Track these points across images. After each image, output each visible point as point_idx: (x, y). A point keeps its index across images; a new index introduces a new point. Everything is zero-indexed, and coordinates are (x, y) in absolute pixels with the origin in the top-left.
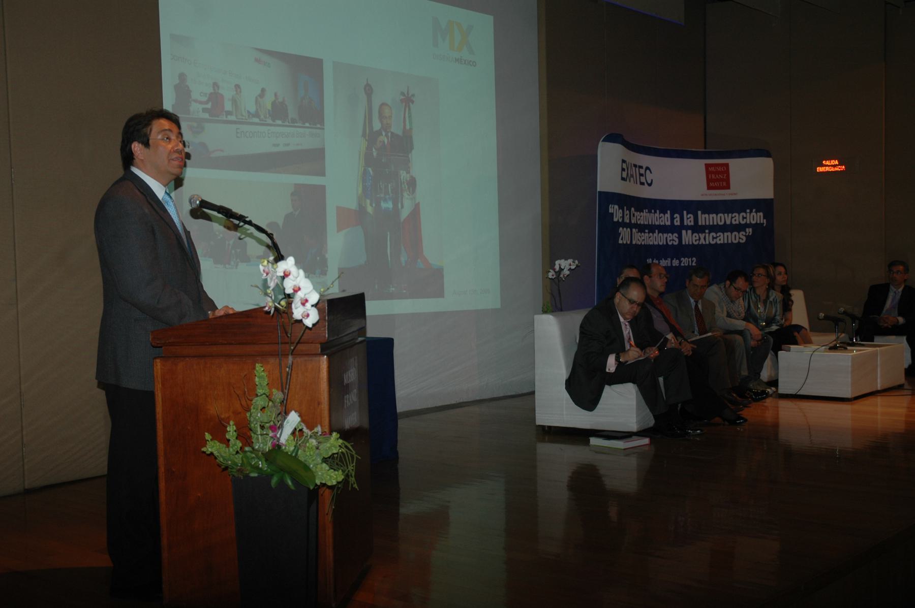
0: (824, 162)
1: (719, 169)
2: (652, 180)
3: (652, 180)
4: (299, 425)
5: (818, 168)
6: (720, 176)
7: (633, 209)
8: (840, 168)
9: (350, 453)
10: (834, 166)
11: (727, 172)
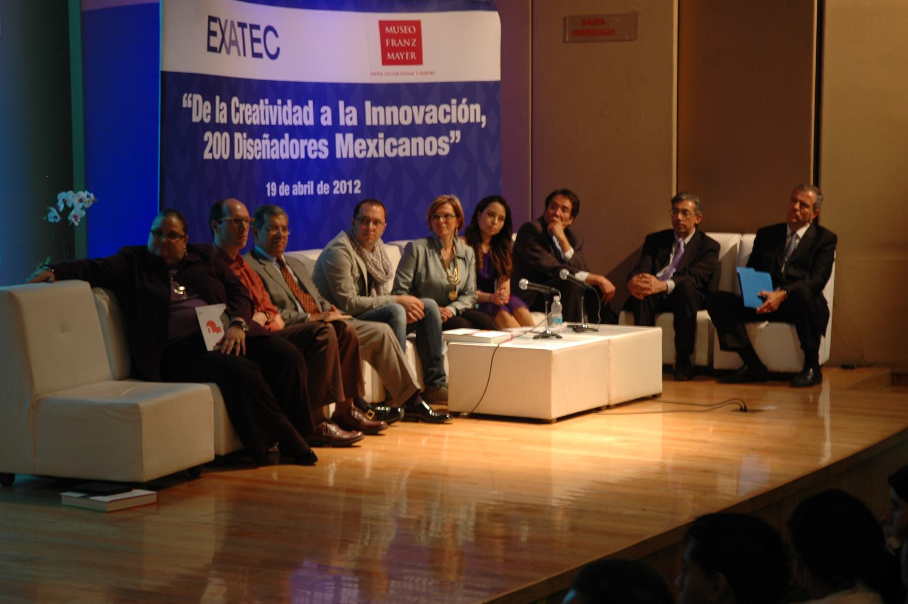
1: (405, 30)
2: (278, 49)
3: (278, 49)
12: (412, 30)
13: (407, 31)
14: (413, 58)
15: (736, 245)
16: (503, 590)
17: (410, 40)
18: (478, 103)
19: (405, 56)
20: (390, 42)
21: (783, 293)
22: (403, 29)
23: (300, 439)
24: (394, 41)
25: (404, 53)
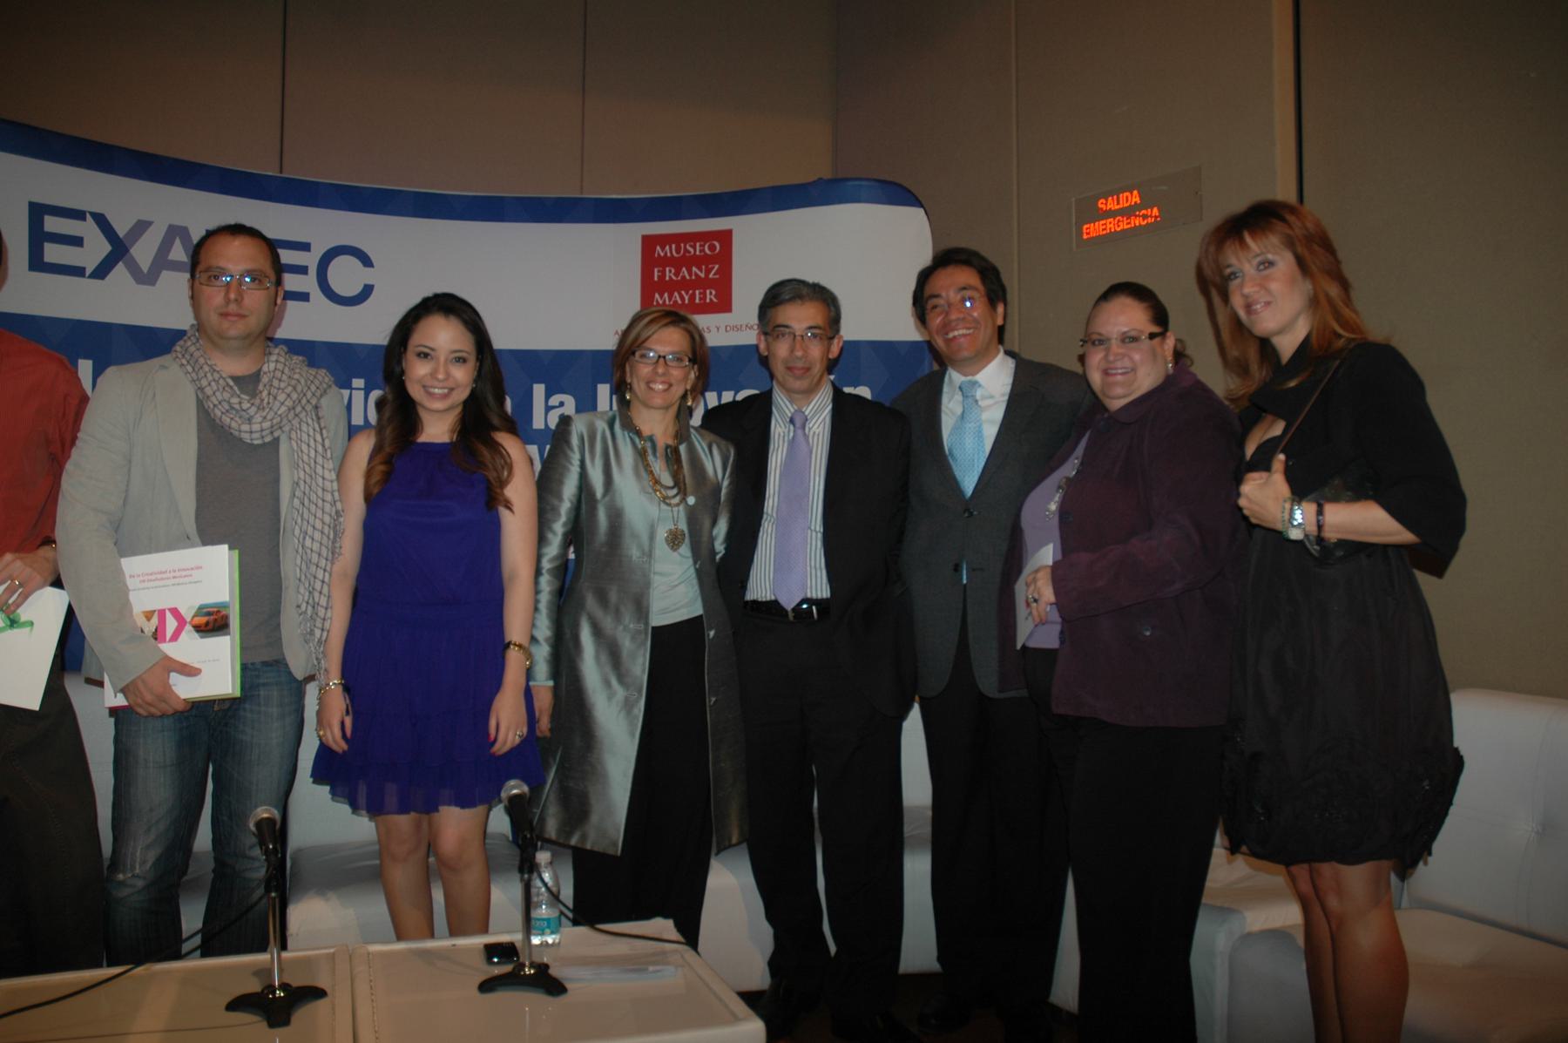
1: (696, 250)
2: (116, 696)
3: (116, 696)
4: (791, 330)
5: (1085, 226)
6: (662, 254)
8: (1145, 217)
9: (701, 271)
10: (1128, 212)
11: (725, 259)
12: (712, 248)
13: (702, 250)
14: (711, 299)
15: (717, 854)
16: (1129, 395)
17: (706, 267)
19: (692, 298)
20: (663, 272)
21: (969, 481)
24: (670, 271)
25: (691, 292)
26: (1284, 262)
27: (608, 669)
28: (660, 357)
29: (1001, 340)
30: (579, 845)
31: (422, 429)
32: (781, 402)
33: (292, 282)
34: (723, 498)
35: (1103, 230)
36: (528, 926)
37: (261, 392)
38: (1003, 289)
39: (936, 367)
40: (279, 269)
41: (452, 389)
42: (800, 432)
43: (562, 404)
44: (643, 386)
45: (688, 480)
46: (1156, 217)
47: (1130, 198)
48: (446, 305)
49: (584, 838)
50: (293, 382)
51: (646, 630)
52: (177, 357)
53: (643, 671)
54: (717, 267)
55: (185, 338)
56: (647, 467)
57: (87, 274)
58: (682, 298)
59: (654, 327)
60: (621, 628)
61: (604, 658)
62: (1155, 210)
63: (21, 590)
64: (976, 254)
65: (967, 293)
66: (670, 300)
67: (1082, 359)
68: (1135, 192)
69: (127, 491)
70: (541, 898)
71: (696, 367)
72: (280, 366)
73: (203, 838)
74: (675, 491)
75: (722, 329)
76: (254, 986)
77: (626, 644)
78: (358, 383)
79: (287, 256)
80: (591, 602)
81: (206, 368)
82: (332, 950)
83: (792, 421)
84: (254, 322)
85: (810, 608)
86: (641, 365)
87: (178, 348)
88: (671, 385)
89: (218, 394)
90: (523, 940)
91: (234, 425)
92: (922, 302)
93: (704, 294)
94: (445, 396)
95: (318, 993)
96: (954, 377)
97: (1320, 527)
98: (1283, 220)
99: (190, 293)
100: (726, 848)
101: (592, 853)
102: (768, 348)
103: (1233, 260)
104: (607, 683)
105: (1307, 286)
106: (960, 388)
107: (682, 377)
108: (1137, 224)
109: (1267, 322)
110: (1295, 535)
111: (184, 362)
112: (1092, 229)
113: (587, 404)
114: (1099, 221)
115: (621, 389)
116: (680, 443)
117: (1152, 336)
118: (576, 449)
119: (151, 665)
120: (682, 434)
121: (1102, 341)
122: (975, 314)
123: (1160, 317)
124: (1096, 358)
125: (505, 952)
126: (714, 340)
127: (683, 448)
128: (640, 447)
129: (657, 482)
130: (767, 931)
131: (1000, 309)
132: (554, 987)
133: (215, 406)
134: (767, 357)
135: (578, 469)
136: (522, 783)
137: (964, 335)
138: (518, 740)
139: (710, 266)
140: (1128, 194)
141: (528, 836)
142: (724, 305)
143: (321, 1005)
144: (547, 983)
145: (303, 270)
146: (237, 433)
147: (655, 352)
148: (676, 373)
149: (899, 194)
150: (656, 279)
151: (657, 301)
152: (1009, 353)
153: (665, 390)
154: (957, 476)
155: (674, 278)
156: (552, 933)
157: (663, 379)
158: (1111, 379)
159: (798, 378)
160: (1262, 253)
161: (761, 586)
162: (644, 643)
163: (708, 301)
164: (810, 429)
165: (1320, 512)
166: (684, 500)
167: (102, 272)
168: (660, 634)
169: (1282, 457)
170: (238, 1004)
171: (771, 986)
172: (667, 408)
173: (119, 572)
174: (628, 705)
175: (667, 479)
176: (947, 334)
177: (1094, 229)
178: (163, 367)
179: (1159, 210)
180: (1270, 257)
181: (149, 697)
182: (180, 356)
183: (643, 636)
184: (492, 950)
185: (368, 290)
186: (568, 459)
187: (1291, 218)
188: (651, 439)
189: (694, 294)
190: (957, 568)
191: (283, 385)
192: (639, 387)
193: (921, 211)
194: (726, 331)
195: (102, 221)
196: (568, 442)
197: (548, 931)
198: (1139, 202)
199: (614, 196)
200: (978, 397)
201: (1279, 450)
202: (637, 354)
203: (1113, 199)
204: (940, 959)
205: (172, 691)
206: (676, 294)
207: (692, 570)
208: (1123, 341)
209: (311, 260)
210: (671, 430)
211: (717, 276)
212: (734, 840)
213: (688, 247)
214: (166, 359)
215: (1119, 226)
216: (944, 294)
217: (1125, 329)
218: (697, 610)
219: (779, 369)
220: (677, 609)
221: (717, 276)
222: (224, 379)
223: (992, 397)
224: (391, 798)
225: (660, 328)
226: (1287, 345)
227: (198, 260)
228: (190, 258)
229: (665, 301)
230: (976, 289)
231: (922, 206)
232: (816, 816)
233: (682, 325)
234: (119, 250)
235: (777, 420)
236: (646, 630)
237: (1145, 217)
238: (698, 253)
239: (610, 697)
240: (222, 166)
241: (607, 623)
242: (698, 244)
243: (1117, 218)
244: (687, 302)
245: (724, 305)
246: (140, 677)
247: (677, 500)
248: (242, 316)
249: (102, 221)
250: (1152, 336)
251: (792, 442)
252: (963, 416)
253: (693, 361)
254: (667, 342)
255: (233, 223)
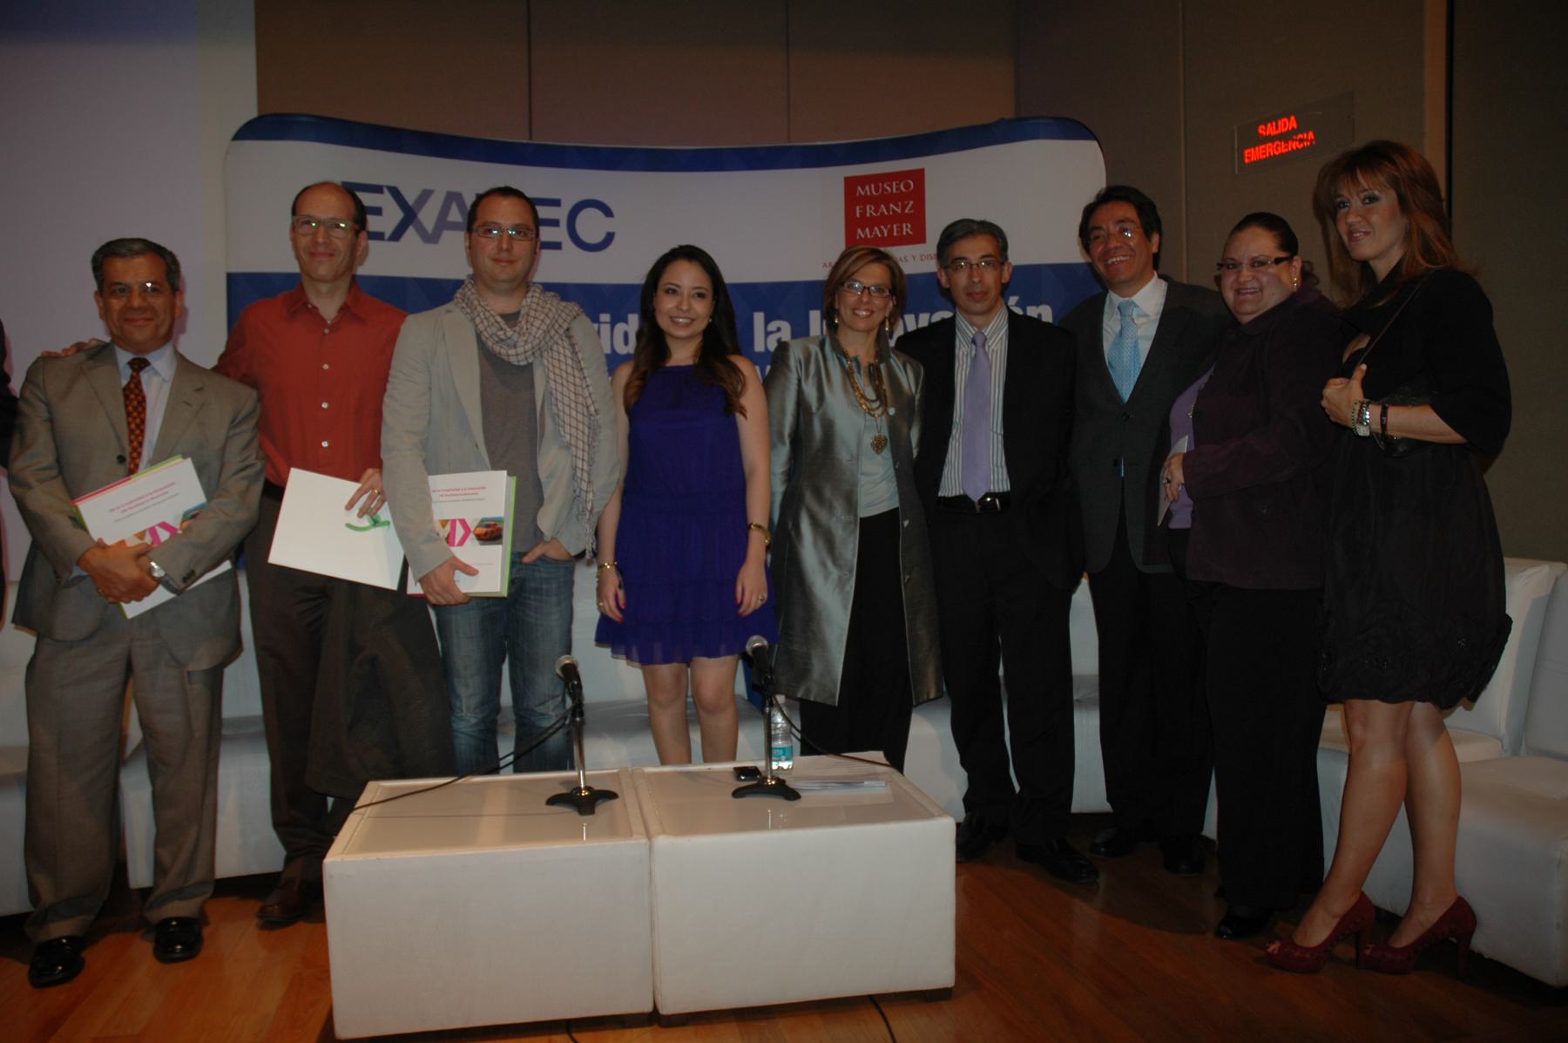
0: (1261, 130)
5: (1246, 152)
6: (863, 236)
7: (1294, 137)
8: (1301, 141)
10: (1286, 137)
11: (918, 195)
12: (907, 186)
13: (898, 189)
16: (1257, 311)
18: (1047, 303)
19: (891, 231)
20: (864, 211)
21: (1126, 389)
22: (891, 186)
23: (916, 403)
25: (889, 226)
26: (1387, 199)
27: (824, 553)
28: (865, 288)
29: (1156, 266)
30: (804, 697)
31: (671, 355)
32: (964, 327)
33: (547, 234)
34: (916, 409)
35: (1263, 154)
36: (770, 754)
37: (520, 322)
38: (1158, 221)
39: (1099, 290)
40: (538, 222)
41: (693, 320)
42: (980, 350)
43: (779, 329)
44: (849, 312)
45: (888, 394)
46: (1311, 140)
47: (1287, 123)
48: (690, 253)
49: (808, 691)
50: (546, 311)
51: (856, 521)
52: (458, 302)
53: (854, 555)
54: (911, 203)
55: (463, 286)
56: (853, 384)
57: (387, 236)
58: (882, 232)
59: (861, 263)
60: (834, 519)
61: (821, 544)
62: (1311, 133)
63: (379, 497)
64: (1137, 192)
65: (1127, 225)
66: (871, 234)
67: (1218, 280)
68: (1292, 118)
69: (430, 414)
70: (778, 731)
71: (894, 298)
72: (535, 300)
73: (506, 697)
74: (878, 404)
75: (918, 258)
76: (563, 790)
77: (839, 532)
78: (605, 317)
79: (543, 212)
80: (809, 498)
81: (479, 309)
82: (616, 771)
83: (974, 341)
84: (520, 266)
85: (993, 501)
86: (849, 295)
87: (458, 295)
88: (872, 312)
89: (488, 329)
90: (766, 767)
91: (503, 351)
92: (1087, 232)
93: (901, 228)
94: (687, 326)
95: (611, 795)
96: (1114, 298)
97: (1384, 426)
98: (1393, 163)
99: (468, 244)
100: (921, 703)
101: (815, 704)
102: (949, 281)
103: (1345, 193)
104: (824, 565)
105: (1402, 222)
106: (1119, 308)
107: (882, 305)
108: (1294, 148)
109: (1366, 248)
110: (1363, 431)
111: (464, 305)
112: (1253, 153)
113: (801, 330)
114: (1259, 145)
115: (830, 315)
116: (880, 362)
117: (1278, 261)
118: (794, 370)
119: (441, 562)
120: (881, 354)
121: (1236, 265)
122: (1132, 244)
123: (1289, 244)
124: (1229, 280)
125: (751, 772)
126: (909, 268)
127: (882, 367)
128: (847, 366)
129: (863, 396)
130: (962, 775)
131: (1155, 238)
132: (792, 795)
133: (487, 338)
134: (948, 290)
135: (796, 387)
136: (761, 638)
137: (1121, 261)
138: (760, 603)
139: (906, 202)
140: (1286, 120)
141: (769, 677)
142: (919, 237)
143: (615, 802)
144: (784, 791)
145: (554, 223)
146: (506, 358)
147: (860, 282)
148: (878, 302)
149: (1072, 129)
150: (858, 215)
151: (860, 235)
152: (1160, 276)
153: (868, 316)
154: (1117, 386)
155: (874, 214)
156: (787, 760)
157: (866, 307)
158: (1242, 297)
159: (978, 301)
160: (1370, 189)
161: (952, 484)
162: (854, 531)
163: (904, 233)
164: (989, 347)
165: (1384, 414)
166: (886, 411)
167: (397, 235)
168: (865, 522)
169: (1364, 367)
170: (553, 801)
171: (966, 819)
172: (868, 332)
173: (426, 482)
174: (841, 584)
175: (871, 395)
176: (1107, 260)
177: (1254, 154)
178: (449, 311)
179: (1314, 134)
180: (1376, 193)
181: (437, 588)
182: (460, 301)
183: (853, 526)
184: (740, 771)
185: (610, 238)
186: (787, 379)
187: (1399, 160)
188: (856, 360)
189: (892, 229)
190: (1116, 463)
191: (537, 314)
192: (846, 313)
193: (1095, 144)
194: (922, 260)
195: (396, 193)
196: (787, 365)
197: (783, 757)
198: (1295, 127)
199: (819, 143)
200: (1134, 316)
201: (1362, 360)
202: (846, 285)
203: (1272, 125)
204: (1109, 799)
205: (455, 585)
206: (876, 228)
207: (892, 470)
208: (1252, 265)
209: (561, 214)
210: (872, 352)
211: (912, 211)
212: (932, 696)
213: (885, 186)
214: (450, 306)
215: (1277, 150)
216: (1104, 227)
217: (1255, 255)
218: (894, 503)
219: (962, 298)
220: (881, 502)
221: (912, 211)
222: (493, 316)
223: (1146, 316)
224: (658, 653)
225: (865, 264)
226: (1382, 268)
227: (474, 220)
228: (466, 217)
229: (866, 235)
230: (1132, 221)
231: (1096, 139)
232: (1002, 681)
233: (885, 261)
234: (410, 215)
235: (960, 341)
236: (856, 521)
237: (1301, 141)
238: (894, 191)
239: (826, 578)
240: (487, 138)
241: (823, 515)
242: (894, 184)
243: (1276, 143)
244: (886, 235)
245: (919, 237)
246: (433, 572)
247: (879, 411)
248: (511, 262)
249: (396, 193)
250: (1278, 261)
251: (975, 359)
252: (1121, 334)
253: (893, 292)
254: (872, 275)
255: (502, 186)
